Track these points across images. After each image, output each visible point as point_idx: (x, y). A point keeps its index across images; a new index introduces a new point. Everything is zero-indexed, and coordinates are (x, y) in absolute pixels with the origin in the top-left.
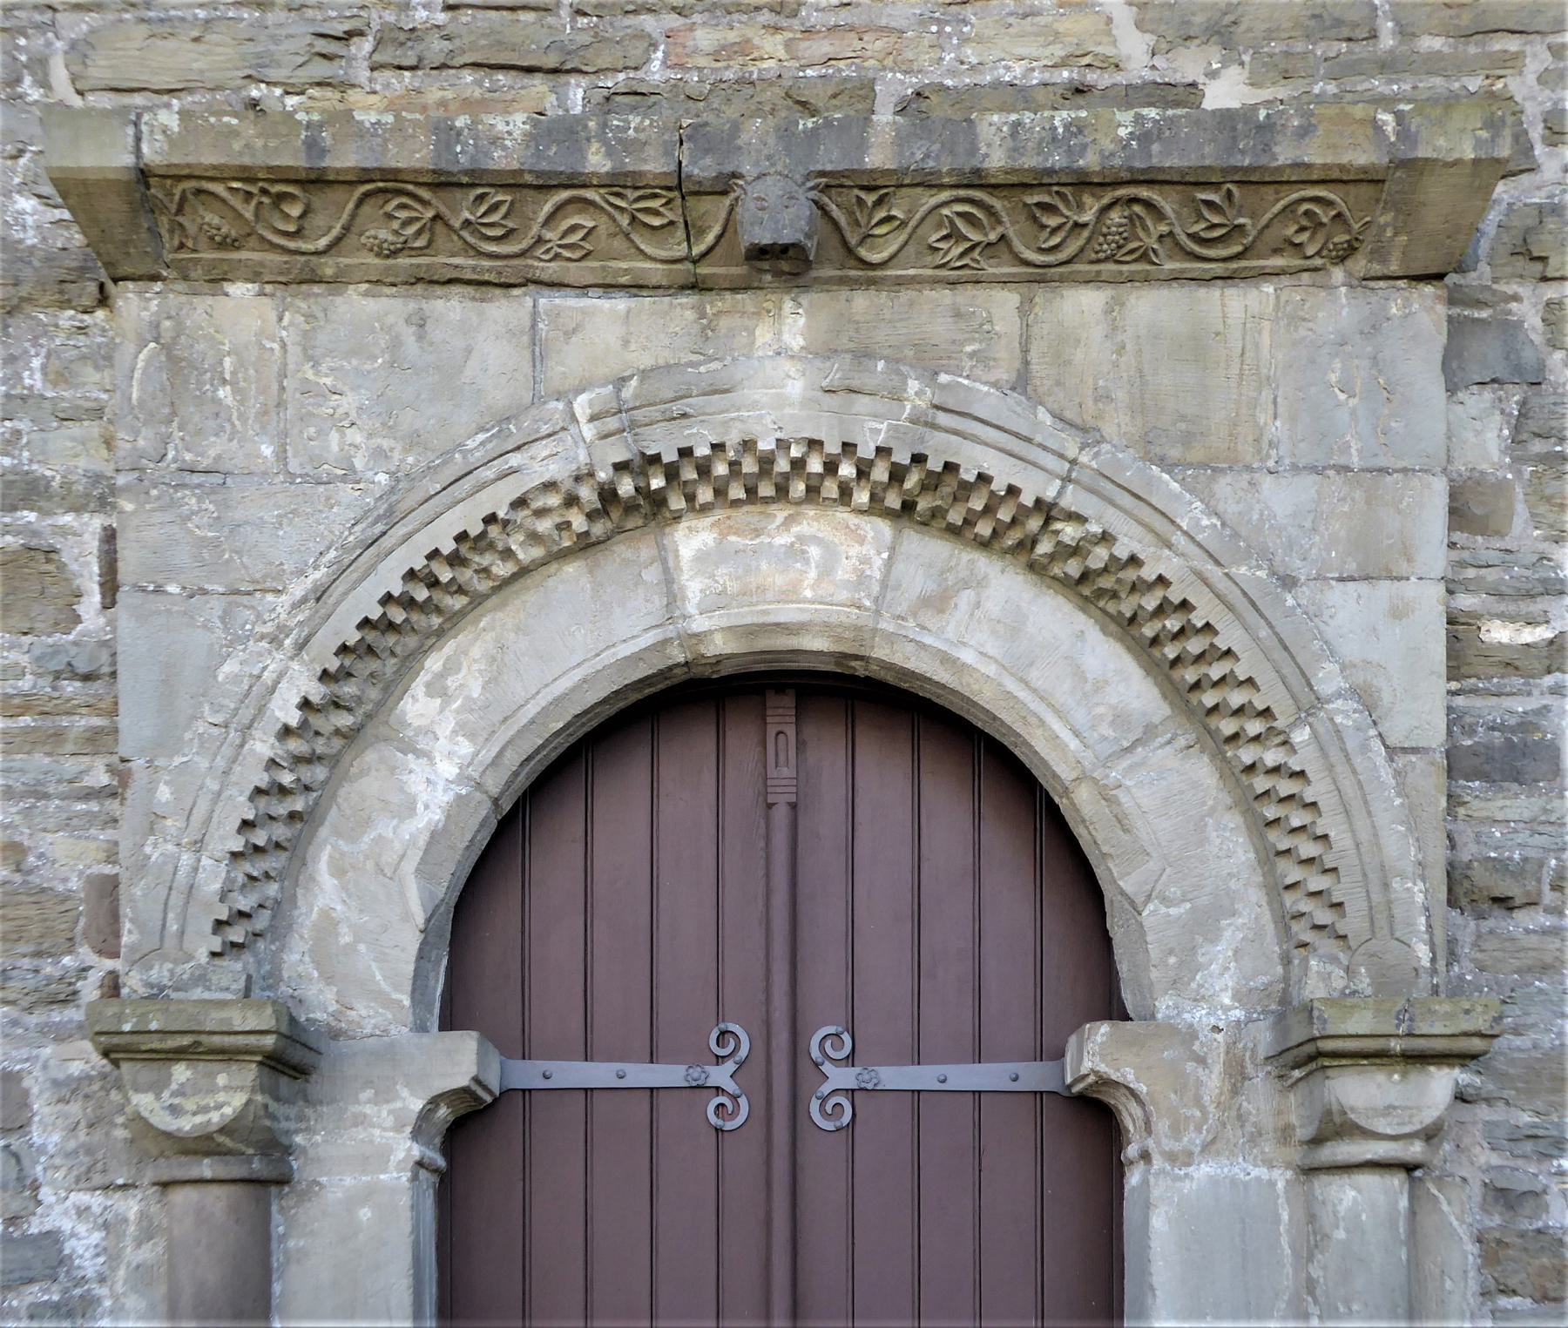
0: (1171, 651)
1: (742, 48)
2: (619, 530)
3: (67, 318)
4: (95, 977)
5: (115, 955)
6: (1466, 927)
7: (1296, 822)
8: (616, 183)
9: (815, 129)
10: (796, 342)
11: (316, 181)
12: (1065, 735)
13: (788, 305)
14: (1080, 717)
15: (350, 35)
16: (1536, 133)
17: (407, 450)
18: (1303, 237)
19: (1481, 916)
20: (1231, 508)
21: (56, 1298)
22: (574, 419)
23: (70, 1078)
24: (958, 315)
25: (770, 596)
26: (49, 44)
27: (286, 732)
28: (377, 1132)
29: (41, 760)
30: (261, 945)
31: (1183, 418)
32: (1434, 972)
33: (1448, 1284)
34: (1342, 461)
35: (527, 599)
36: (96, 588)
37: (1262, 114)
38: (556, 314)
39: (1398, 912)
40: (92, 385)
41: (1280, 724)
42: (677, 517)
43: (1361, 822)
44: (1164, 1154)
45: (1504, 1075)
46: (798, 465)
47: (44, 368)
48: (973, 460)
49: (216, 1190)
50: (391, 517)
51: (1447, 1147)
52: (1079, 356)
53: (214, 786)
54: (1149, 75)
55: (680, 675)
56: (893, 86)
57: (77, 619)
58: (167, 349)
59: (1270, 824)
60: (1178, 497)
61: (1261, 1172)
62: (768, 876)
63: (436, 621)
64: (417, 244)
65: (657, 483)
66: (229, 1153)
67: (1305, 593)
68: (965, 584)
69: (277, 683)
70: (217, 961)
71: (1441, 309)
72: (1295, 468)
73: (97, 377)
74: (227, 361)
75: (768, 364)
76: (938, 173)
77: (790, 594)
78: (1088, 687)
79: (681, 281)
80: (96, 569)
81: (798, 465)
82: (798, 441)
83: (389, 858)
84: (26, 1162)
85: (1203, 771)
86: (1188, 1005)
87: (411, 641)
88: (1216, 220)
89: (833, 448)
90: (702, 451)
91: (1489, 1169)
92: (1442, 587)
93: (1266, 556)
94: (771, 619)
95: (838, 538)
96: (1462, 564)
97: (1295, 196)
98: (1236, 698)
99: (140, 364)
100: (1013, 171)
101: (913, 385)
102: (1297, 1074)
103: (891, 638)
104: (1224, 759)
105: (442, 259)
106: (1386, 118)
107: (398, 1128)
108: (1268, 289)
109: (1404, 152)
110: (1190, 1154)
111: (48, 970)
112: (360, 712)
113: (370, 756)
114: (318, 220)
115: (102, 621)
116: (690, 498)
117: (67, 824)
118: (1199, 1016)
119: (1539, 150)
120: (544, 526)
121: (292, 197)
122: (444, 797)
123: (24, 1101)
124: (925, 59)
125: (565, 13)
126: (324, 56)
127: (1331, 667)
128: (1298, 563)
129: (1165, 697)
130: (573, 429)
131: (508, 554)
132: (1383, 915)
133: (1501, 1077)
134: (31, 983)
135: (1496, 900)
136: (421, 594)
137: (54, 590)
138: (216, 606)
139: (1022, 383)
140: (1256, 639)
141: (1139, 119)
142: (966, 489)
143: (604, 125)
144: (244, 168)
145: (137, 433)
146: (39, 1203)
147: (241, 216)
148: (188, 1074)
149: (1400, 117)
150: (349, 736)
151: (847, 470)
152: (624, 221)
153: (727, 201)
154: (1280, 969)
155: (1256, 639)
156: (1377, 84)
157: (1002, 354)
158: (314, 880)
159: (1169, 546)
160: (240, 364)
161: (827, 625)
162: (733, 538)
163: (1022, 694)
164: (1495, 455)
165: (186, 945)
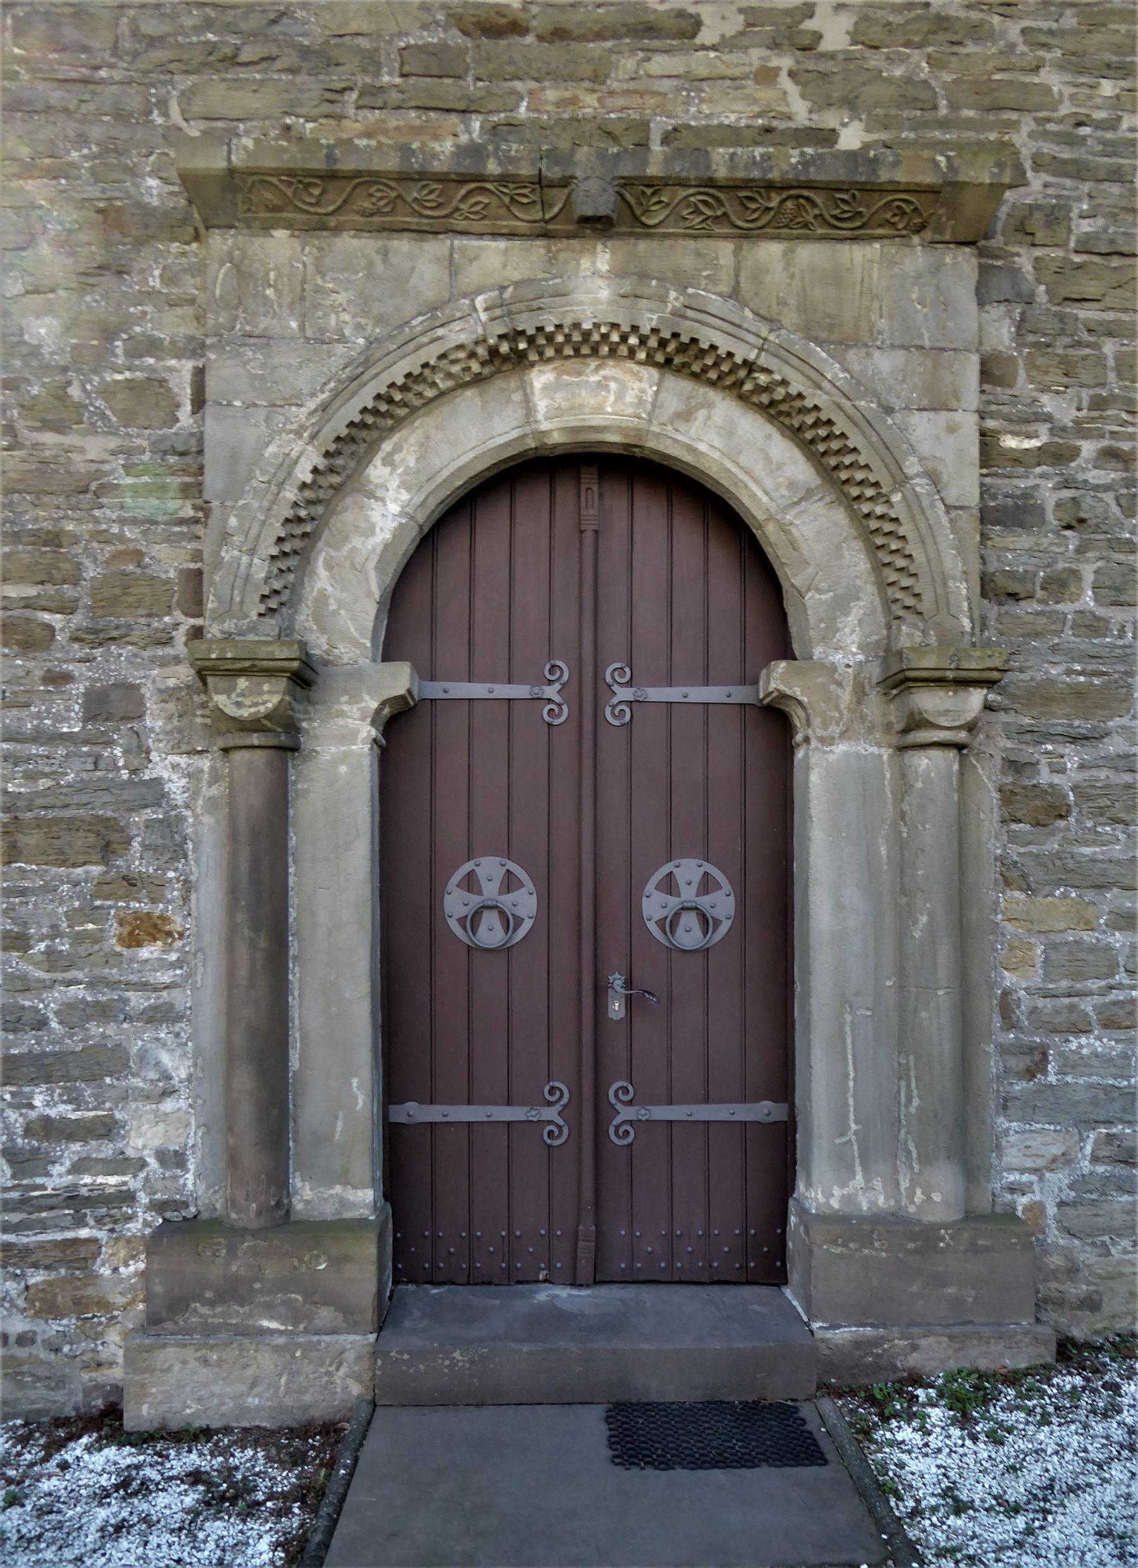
0: (821, 448)
1: (574, 101)
2: (498, 371)
3: (175, 247)
4: (183, 629)
5: (200, 615)
6: (992, 610)
7: (893, 547)
8: (504, 179)
9: (618, 155)
12: (760, 493)
13: (600, 247)
14: (769, 483)
15: (345, 90)
16: (1028, 165)
17: (376, 325)
18: (896, 219)
19: (1001, 604)
20: (856, 368)
22: (476, 310)
23: (168, 688)
24: (698, 254)
25: (587, 410)
26: (169, 92)
27: (304, 486)
29: (154, 502)
30: (284, 610)
31: (828, 316)
32: (973, 634)
33: (982, 816)
34: (919, 343)
35: (442, 412)
36: (189, 402)
37: (872, 153)
38: (463, 250)
39: (952, 599)
40: (190, 286)
42: (532, 365)
43: (930, 548)
44: (817, 738)
45: (1014, 695)
46: (605, 337)
47: (161, 276)
48: (708, 336)
49: (259, 752)
50: (367, 364)
51: (981, 736)
52: (768, 279)
54: (807, 123)
55: (532, 455)
56: (660, 124)
57: (177, 420)
58: (237, 267)
59: (879, 548)
60: (825, 361)
61: (874, 750)
62: (581, 572)
63: (390, 422)
64: (386, 210)
65: (522, 346)
66: (269, 730)
67: (898, 417)
68: (702, 406)
69: (298, 458)
70: (262, 619)
71: (974, 261)
72: (892, 346)
73: (192, 281)
75: (589, 280)
76: (689, 179)
77: (599, 409)
78: (774, 467)
80: (189, 391)
81: (605, 337)
82: (605, 324)
83: (359, 560)
84: (143, 737)
85: (840, 516)
86: (831, 651)
87: (375, 434)
88: (846, 208)
89: (626, 328)
90: (550, 328)
91: (1005, 750)
92: (976, 417)
93: (875, 395)
95: (627, 378)
96: (989, 403)
97: (890, 198)
98: (859, 476)
99: (221, 275)
100: (732, 179)
101: (673, 294)
102: (894, 692)
103: (657, 436)
104: (853, 510)
106: (941, 159)
107: (363, 719)
108: (877, 246)
109: (951, 177)
110: (833, 738)
111: (156, 624)
112: (344, 475)
113: (349, 501)
114: (330, 196)
115: (191, 421)
116: (541, 354)
117: (169, 539)
118: (838, 658)
119: (1030, 174)
120: (455, 369)
122: (392, 524)
123: (141, 701)
124: (679, 110)
125: (470, 79)
127: (913, 459)
128: (894, 400)
129: (818, 473)
130: (475, 315)
131: (433, 384)
132: (944, 601)
133: (1013, 697)
134: (146, 631)
135: (1010, 595)
136: (383, 407)
138: (262, 413)
139: (735, 294)
140: (870, 442)
141: (802, 154)
142: (702, 353)
143: (497, 149)
144: (290, 169)
145: (218, 314)
149: (948, 158)
150: (336, 488)
151: (633, 340)
152: (507, 200)
153: (566, 191)
154: (885, 632)
155: (870, 442)
156: (937, 134)
159: (820, 388)
160: (279, 275)
161: (619, 427)
162: (565, 377)
163: (735, 469)
164: (1007, 342)
165: (245, 609)
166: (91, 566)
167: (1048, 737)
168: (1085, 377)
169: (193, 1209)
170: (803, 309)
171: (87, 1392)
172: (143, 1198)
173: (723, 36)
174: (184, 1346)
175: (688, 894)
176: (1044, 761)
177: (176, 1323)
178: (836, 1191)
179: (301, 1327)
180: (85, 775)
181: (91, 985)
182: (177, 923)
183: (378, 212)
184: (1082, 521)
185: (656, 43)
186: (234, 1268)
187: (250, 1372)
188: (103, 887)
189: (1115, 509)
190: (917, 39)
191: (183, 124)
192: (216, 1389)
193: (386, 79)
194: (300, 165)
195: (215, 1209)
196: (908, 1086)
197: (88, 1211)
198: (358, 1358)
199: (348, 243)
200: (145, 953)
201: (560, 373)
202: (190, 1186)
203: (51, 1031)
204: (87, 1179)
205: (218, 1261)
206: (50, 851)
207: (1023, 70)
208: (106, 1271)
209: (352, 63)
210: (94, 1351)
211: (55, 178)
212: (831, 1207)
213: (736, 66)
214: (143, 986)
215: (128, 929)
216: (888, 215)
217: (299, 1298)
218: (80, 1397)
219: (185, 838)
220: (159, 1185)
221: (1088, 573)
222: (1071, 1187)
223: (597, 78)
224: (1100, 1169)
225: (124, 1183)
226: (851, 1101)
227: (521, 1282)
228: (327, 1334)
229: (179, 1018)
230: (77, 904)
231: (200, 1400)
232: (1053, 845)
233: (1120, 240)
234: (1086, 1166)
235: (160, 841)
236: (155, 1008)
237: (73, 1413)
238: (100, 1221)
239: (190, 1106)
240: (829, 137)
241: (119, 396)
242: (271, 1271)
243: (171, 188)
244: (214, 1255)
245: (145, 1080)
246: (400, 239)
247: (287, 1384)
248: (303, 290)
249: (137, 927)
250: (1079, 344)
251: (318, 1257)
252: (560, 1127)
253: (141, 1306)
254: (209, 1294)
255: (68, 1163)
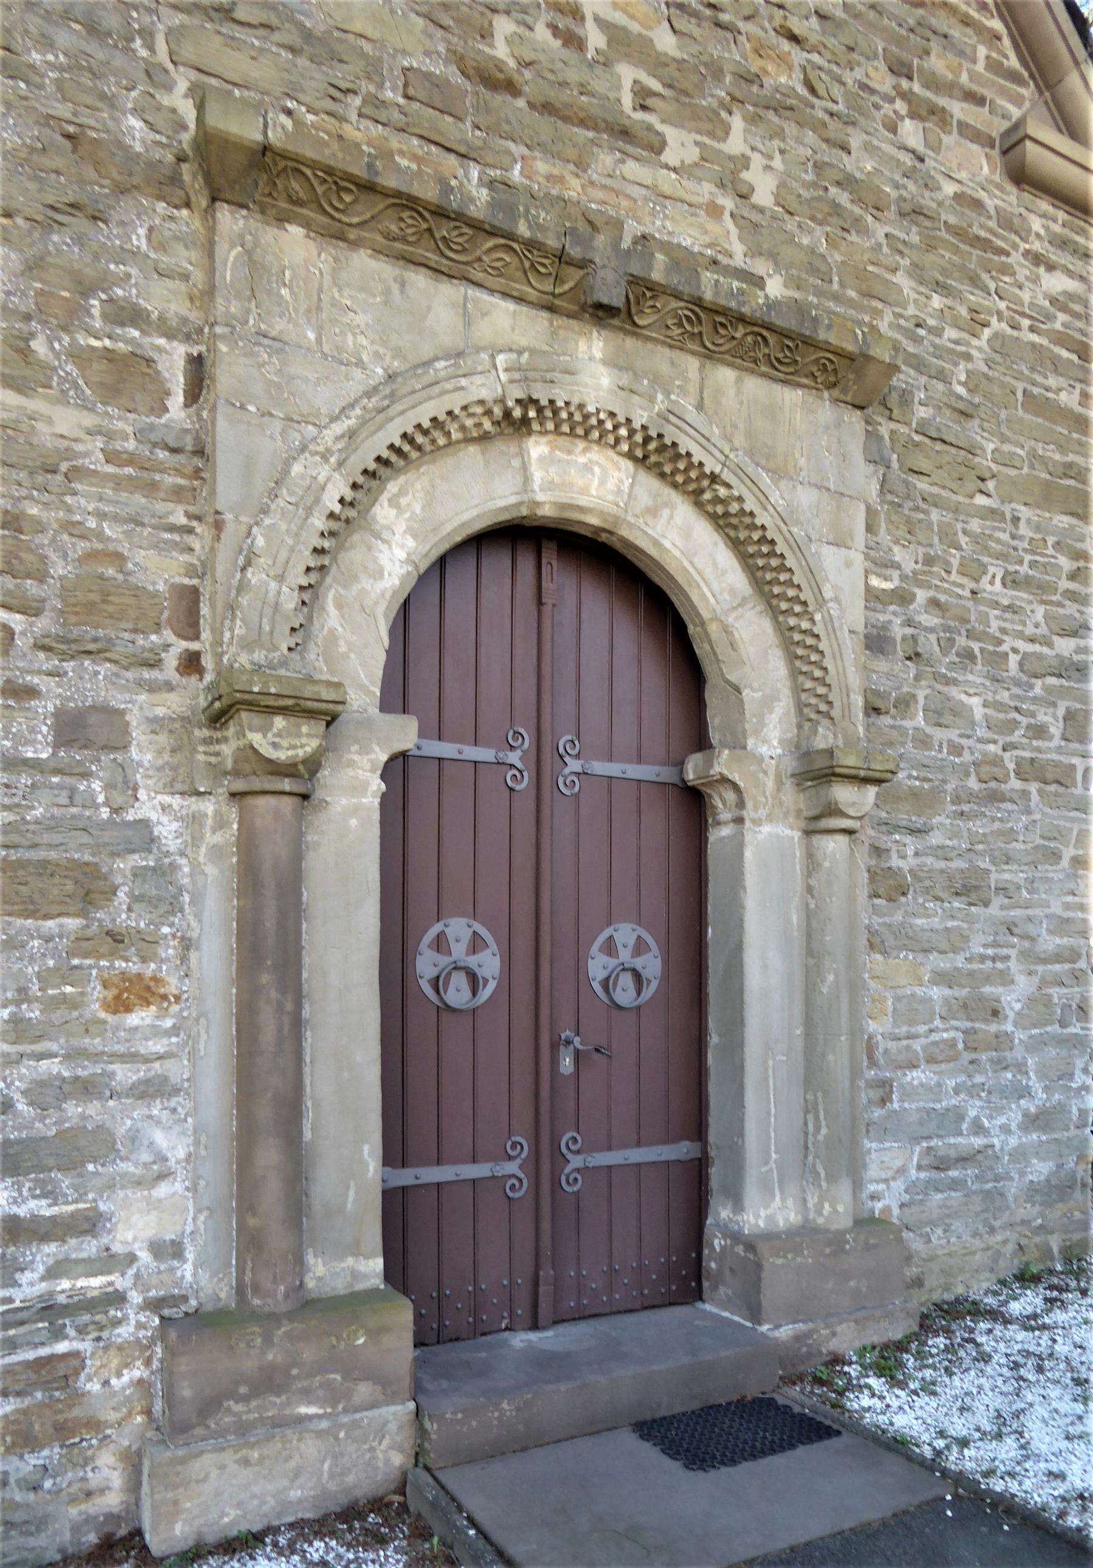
1: (560, 179)
2: (501, 434)
3: (161, 206)
8: (531, 245)
10: (599, 355)
11: (369, 188)
14: (716, 587)
17: (394, 358)
21: (152, 864)
24: (673, 363)
28: (360, 772)
29: (139, 499)
36: (181, 393)
38: (476, 301)
41: (810, 609)
48: (686, 444)
53: (290, 542)
57: (167, 410)
58: (249, 253)
61: (788, 832)
64: (411, 239)
74: (287, 273)
76: (681, 292)
77: (585, 491)
79: (544, 303)
80: (182, 380)
83: (368, 603)
84: (128, 771)
85: (766, 625)
89: (621, 419)
91: (871, 838)
94: (575, 502)
97: (821, 354)
99: (231, 259)
101: (660, 397)
103: (631, 525)
105: (420, 251)
107: (373, 771)
108: (800, 392)
111: (141, 642)
113: (356, 537)
114: (359, 208)
115: (183, 414)
118: (764, 750)
120: (469, 422)
121: (350, 191)
123: (125, 730)
125: (468, 124)
126: (333, 98)
131: (448, 434)
137: (151, 387)
144: (330, 167)
146: (137, 799)
147: (314, 189)
148: (284, 723)
152: (527, 264)
153: (581, 273)
157: (692, 390)
158: (324, 609)
159: (766, 509)
160: (294, 276)
161: (602, 512)
162: (557, 453)
163: (691, 570)
166: (61, 563)
167: (897, 828)
168: (921, 537)
169: (193, 1303)
170: (749, 435)
171: (76, 1529)
172: (135, 1298)
173: (683, 162)
174: (223, 1449)
175: (625, 955)
176: (894, 848)
177: (207, 1427)
178: (763, 1213)
179: (340, 1407)
180: (56, 811)
181: (69, 1057)
182: (173, 984)
183: (404, 240)
184: (918, 655)
185: (629, 148)
186: (270, 1357)
187: (292, 1464)
188: (82, 944)
189: (937, 648)
190: (819, 216)
191: (170, 67)
192: (256, 1489)
193: (389, 94)
194: (340, 165)
195: (220, 1299)
196: (817, 1118)
197: (67, 1322)
198: (400, 1428)
199: (363, 261)
200: (134, 1019)
201: (553, 447)
202: (189, 1277)
203: (17, 1114)
204: (65, 1284)
205: (252, 1352)
206: (17, 899)
207: (886, 268)
208: (95, 1387)
209: (356, 66)
210: (84, 1479)
211: (11, 77)
212: (758, 1226)
213: (693, 193)
214: (131, 1057)
215: (114, 991)
216: (814, 369)
217: (338, 1377)
218: (67, 1536)
219: (181, 890)
220: (154, 1281)
221: (921, 695)
222: (906, 1191)
223: (581, 165)
224: (923, 1175)
225: (111, 1284)
226: (772, 1135)
227: (484, 1334)
228: (366, 1409)
229: (176, 1091)
230: (51, 963)
231: (239, 1505)
232: (898, 917)
233: (944, 429)
234: (913, 1173)
235: (154, 892)
236: (147, 1082)
237: (58, 1557)
238: (82, 1331)
239: (187, 1189)
240: (759, 282)
241: (95, 366)
242: (309, 1354)
243: (158, 137)
244: (249, 1346)
245: (136, 1164)
246: (416, 273)
247: (330, 1469)
248: (320, 299)
249: (127, 990)
250: (917, 509)
251: (355, 1332)
252: (520, 1180)
253: (139, 1419)
254: (243, 1390)
255: (41, 1269)
